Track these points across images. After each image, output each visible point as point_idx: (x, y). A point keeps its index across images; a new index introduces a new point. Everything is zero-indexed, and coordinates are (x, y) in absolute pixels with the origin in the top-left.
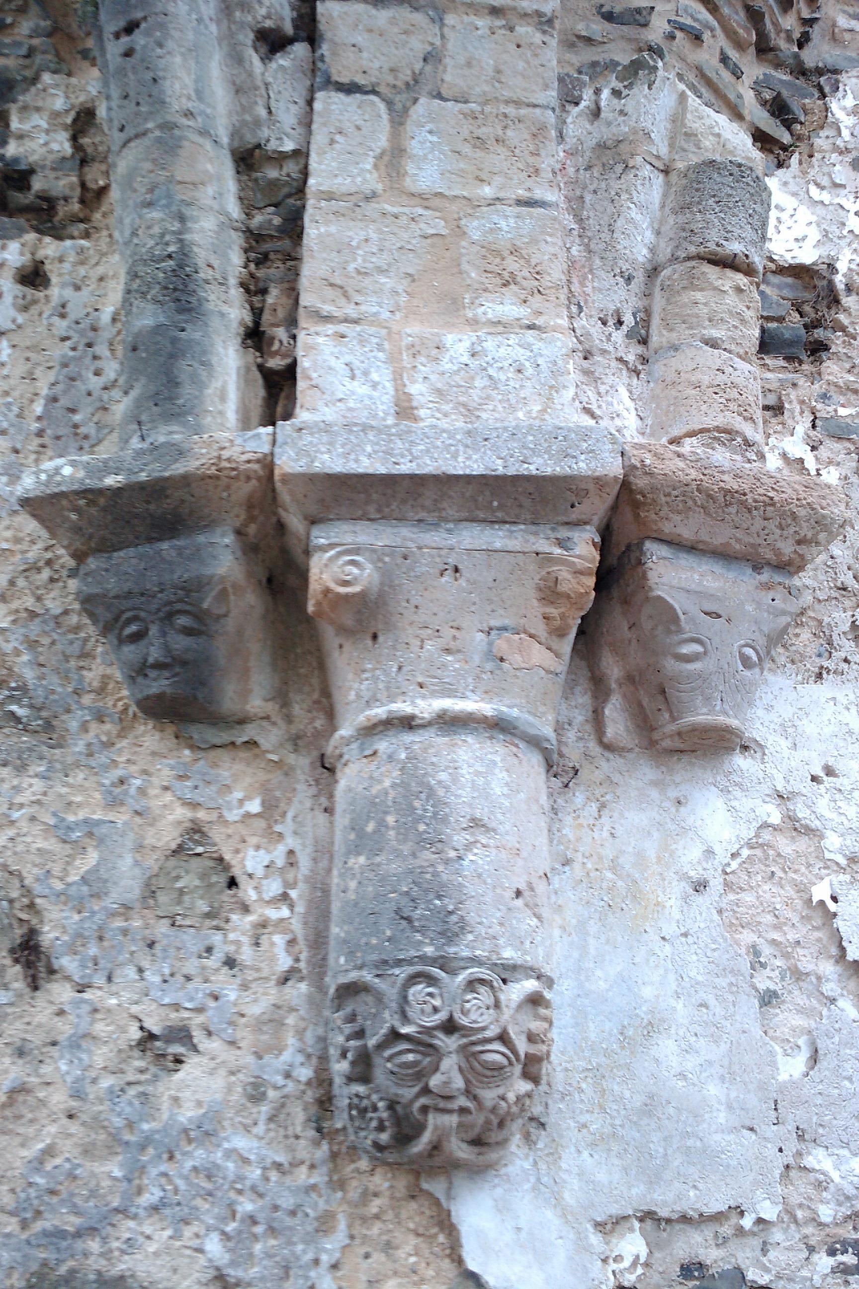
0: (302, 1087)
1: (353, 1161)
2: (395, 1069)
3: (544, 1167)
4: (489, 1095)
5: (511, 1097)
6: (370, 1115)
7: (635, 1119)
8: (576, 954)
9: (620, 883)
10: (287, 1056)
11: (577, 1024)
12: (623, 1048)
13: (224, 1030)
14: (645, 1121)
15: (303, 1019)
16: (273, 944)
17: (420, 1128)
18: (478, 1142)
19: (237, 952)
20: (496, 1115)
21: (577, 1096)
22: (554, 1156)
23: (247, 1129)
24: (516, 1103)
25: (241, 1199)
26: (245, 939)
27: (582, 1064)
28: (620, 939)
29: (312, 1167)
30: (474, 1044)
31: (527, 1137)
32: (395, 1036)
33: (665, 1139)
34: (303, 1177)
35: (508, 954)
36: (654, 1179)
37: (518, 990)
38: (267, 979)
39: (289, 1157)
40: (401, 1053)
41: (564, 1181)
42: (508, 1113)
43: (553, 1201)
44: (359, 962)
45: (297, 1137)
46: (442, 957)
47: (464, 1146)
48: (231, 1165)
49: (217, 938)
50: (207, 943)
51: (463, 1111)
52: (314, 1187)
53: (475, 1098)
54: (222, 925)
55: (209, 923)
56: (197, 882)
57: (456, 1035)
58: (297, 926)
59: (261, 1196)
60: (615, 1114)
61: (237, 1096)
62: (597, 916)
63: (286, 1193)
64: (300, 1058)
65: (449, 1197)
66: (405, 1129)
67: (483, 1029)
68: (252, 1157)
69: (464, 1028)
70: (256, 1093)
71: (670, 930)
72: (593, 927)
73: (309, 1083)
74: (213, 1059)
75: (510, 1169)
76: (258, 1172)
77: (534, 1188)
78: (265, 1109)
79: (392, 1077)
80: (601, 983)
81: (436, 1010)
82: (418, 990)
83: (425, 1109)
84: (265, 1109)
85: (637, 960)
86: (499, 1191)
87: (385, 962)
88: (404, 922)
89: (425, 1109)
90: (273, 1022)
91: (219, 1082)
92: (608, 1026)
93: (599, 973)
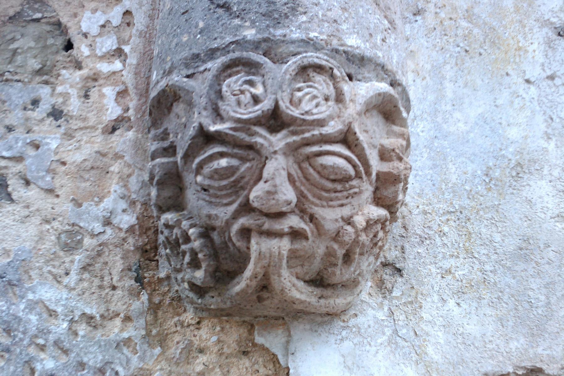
0: (122, 235)
1: (179, 315)
2: (207, 182)
3: (402, 317)
4: (330, 216)
5: (360, 221)
6: (183, 247)
7: (509, 264)
8: (431, 97)
9: (476, 31)
10: (108, 203)
11: (435, 166)
12: (490, 189)
13: (43, 178)
14: (521, 266)
15: (129, 166)
16: (102, 96)
17: (243, 259)
18: (319, 282)
19: (64, 103)
20: (342, 244)
21: (438, 240)
22: (414, 305)
23: (57, 279)
24: (365, 229)
25: (42, 355)
26: (74, 92)
27: (443, 206)
28: (479, 82)
29: (128, 319)
30: (308, 143)
31: (381, 285)
32: (206, 138)
33: (546, 286)
34: (116, 330)
35: (353, 42)
36: (536, 332)
37: (365, 89)
38: (94, 128)
39: (102, 309)
40: (211, 158)
41: (427, 334)
42: (356, 242)
43: (415, 357)
44: (167, 67)
45: (114, 288)
46: (266, 40)
47: (300, 284)
48: (34, 318)
49: (45, 91)
50: (33, 96)
51: (296, 234)
52: (128, 342)
53: (312, 218)
54: (52, 80)
55: (38, 79)
56: (32, 44)
57: (284, 132)
58: (128, 77)
59: (66, 352)
60: (484, 258)
61: (50, 244)
62: (453, 61)
63: (94, 349)
64: (123, 205)
65: (287, 352)
66: (225, 263)
67: (321, 123)
68: (59, 310)
69: (293, 121)
70: (71, 241)
71: (534, 73)
72: (449, 72)
73: (131, 230)
74: (28, 207)
75: (361, 320)
76: (65, 325)
77: (390, 342)
78: (79, 258)
79: (203, 195)
80: (460, 124)
81: (256, 100)
82: (233, 83)
83: (246, 233)
84: (79, 258)
85: (499, 102)
86: (347, 344)
87: (196, 57)
88: (220, 11)
89: (246, 233)
90: (97, 168)
91: (31, 230)
92: (470, 168)
93: (457, 115)
